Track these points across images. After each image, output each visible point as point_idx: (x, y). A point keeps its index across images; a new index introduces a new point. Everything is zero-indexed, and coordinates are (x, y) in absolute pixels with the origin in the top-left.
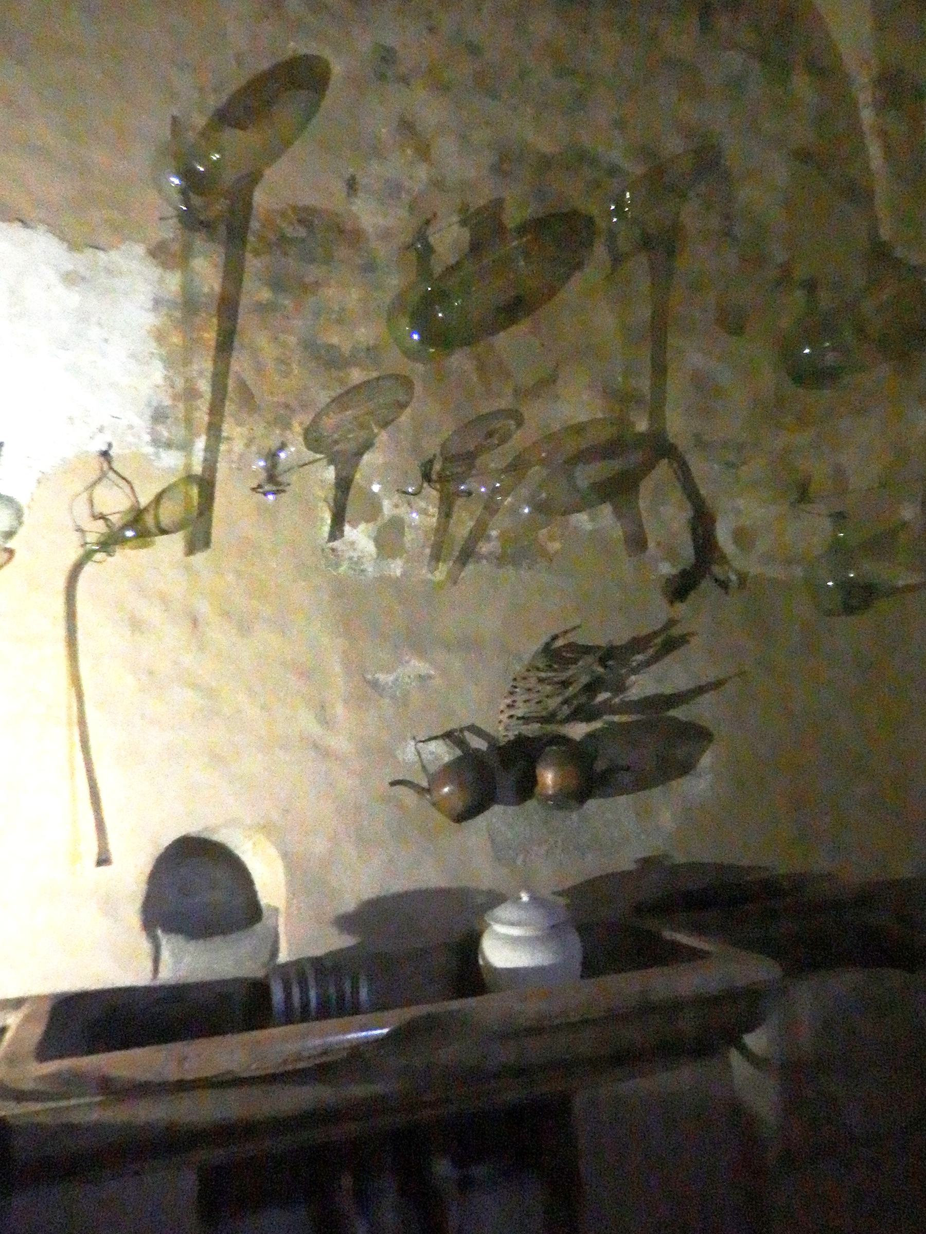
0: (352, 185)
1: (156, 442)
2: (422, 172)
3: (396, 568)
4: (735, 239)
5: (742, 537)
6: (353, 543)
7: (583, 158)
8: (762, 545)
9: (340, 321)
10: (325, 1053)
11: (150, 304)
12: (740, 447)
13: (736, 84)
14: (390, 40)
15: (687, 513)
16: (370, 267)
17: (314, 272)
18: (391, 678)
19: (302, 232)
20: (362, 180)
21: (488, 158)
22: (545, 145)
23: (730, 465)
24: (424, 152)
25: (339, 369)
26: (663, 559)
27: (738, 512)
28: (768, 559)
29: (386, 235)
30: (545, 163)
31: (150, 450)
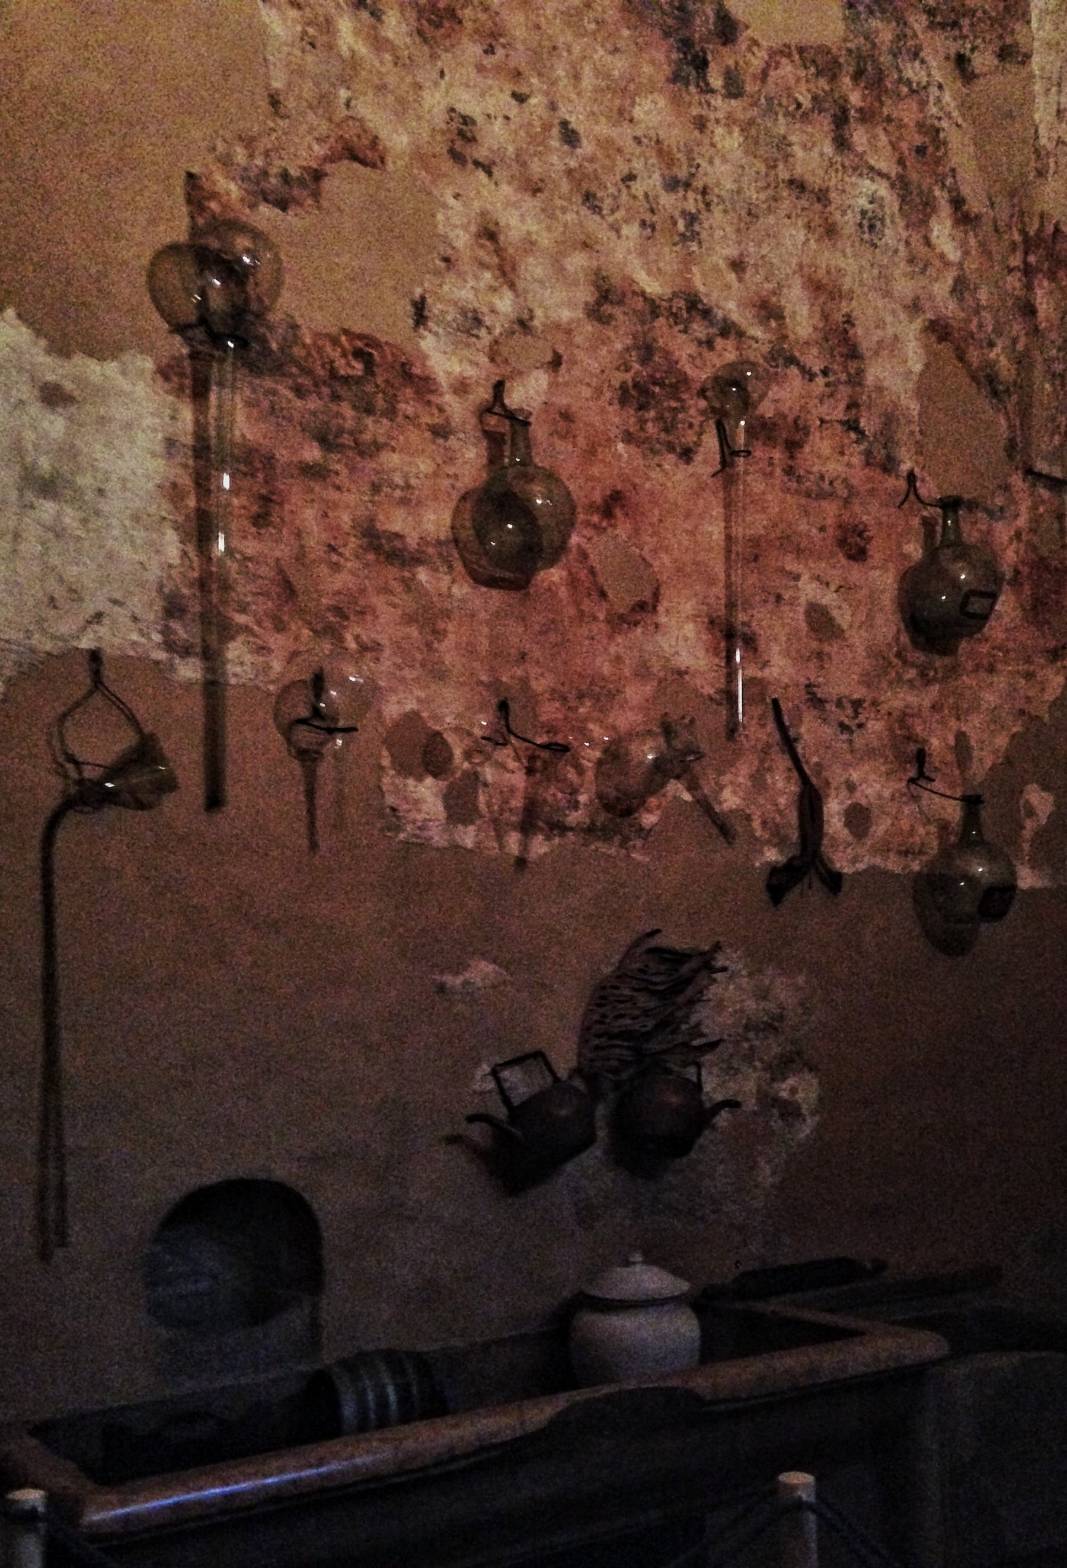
0: (420, 313)
1: (169, 645)
2: (505, 303)
3: (468, 837)
4: (861, 432)
5: (858, 818)
6: (417, 802)
7: (695, 307)
8: (881, 828)
9: (404, 502)
10: (926, 204)
11: (159, 448)
12: (857, 704)
13: (871, 223)
14: (469, 104)
15: (794, 788)
16: (441, 432)
17: (374, 428)
18: (459, 980)
19: (358, 368)
20: (435, 308)
21: (585, 294)
22: (653, 287)
23: (843, 727)
24: (507, 273)
25: (403, 564)
26: (768, 842)
27: (851, 787)
28: (884, 848)
29: (461, 387)
30: (654, 307)
31: (161, 655)
